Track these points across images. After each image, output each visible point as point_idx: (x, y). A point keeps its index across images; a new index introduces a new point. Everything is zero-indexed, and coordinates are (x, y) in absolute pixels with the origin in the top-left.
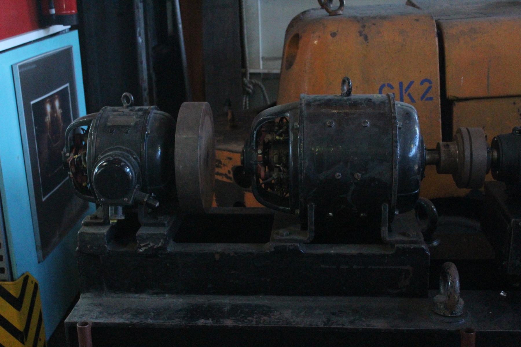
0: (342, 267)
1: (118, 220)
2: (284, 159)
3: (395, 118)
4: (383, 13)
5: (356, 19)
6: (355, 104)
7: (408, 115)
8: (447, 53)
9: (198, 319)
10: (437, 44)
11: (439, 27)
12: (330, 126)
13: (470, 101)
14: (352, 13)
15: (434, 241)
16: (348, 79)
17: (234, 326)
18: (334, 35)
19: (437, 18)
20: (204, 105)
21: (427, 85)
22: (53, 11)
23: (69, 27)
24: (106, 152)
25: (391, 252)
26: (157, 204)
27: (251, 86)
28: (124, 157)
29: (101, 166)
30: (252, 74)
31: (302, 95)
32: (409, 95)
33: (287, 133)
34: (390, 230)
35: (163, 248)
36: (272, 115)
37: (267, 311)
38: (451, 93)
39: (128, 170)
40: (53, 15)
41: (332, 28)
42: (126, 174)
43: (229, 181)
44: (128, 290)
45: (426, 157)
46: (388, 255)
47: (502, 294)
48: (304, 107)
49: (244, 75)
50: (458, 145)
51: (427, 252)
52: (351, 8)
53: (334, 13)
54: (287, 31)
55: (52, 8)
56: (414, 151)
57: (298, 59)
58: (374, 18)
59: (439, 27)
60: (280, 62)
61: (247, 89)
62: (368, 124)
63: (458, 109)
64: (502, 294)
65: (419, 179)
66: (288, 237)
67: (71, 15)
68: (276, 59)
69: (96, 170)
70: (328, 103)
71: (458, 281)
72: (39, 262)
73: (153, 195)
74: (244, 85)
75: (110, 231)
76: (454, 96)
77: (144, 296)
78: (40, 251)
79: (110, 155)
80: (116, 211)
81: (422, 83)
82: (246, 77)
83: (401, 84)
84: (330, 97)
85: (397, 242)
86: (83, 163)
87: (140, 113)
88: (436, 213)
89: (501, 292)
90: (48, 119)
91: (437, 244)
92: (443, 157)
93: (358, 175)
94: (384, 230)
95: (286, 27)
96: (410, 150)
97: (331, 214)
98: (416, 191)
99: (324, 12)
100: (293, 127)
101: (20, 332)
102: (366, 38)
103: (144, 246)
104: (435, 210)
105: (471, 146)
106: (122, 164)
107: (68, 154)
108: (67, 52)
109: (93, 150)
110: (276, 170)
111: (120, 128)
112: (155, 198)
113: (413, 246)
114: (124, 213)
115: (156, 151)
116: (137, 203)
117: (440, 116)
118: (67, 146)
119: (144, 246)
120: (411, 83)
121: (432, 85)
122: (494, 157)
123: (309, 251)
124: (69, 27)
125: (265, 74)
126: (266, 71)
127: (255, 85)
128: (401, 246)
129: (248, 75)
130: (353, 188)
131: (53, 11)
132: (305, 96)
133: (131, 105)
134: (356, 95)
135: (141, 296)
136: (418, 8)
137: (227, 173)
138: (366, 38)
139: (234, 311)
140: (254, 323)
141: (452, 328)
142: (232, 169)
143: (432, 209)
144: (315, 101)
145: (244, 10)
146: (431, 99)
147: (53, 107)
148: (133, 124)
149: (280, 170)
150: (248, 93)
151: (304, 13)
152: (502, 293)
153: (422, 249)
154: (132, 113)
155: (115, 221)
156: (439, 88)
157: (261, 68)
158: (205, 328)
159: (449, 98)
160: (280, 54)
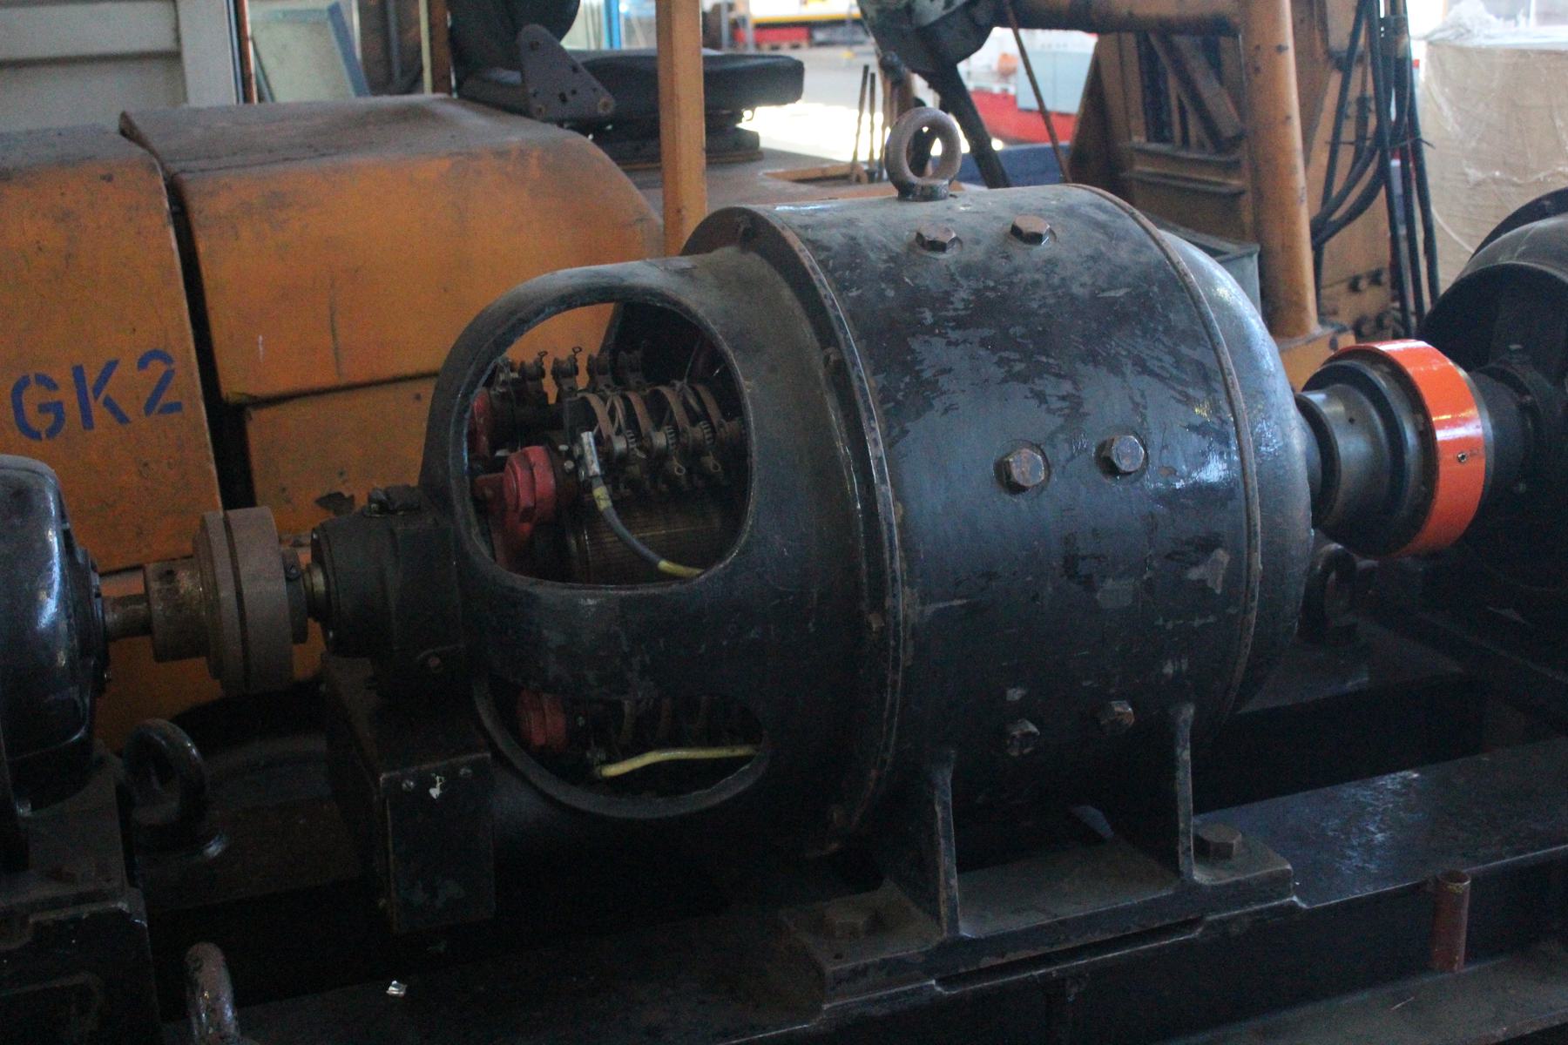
10: (174, 245)
13: (291, 403)
15: (208, 845)
21: (157, 368)
32: (108, 403)
45: (103, 618)
47: (393, 990)
50: (201, 570)
51: (137, 921)
63: (259, 428)
64: (393, 990)
65: (76, 697)
71: (227, 1006)
76: (244, 394)
81: (143, 363)
83: (78, 372)
88: (200, 760)
89: (390, 984)
91: (220, 850)
92: (158, 607)
96: (34, 606)
98: (76, 737)
104: (194, 751)
113: (85, 911)
117: (211, 454)
120: (111, 366)
121: (173, 366)
122: (315, 589)
143: (188, 750)
146: (175, 407)
152: (395, 986)
156: (197, 375)
159: (227, 398)
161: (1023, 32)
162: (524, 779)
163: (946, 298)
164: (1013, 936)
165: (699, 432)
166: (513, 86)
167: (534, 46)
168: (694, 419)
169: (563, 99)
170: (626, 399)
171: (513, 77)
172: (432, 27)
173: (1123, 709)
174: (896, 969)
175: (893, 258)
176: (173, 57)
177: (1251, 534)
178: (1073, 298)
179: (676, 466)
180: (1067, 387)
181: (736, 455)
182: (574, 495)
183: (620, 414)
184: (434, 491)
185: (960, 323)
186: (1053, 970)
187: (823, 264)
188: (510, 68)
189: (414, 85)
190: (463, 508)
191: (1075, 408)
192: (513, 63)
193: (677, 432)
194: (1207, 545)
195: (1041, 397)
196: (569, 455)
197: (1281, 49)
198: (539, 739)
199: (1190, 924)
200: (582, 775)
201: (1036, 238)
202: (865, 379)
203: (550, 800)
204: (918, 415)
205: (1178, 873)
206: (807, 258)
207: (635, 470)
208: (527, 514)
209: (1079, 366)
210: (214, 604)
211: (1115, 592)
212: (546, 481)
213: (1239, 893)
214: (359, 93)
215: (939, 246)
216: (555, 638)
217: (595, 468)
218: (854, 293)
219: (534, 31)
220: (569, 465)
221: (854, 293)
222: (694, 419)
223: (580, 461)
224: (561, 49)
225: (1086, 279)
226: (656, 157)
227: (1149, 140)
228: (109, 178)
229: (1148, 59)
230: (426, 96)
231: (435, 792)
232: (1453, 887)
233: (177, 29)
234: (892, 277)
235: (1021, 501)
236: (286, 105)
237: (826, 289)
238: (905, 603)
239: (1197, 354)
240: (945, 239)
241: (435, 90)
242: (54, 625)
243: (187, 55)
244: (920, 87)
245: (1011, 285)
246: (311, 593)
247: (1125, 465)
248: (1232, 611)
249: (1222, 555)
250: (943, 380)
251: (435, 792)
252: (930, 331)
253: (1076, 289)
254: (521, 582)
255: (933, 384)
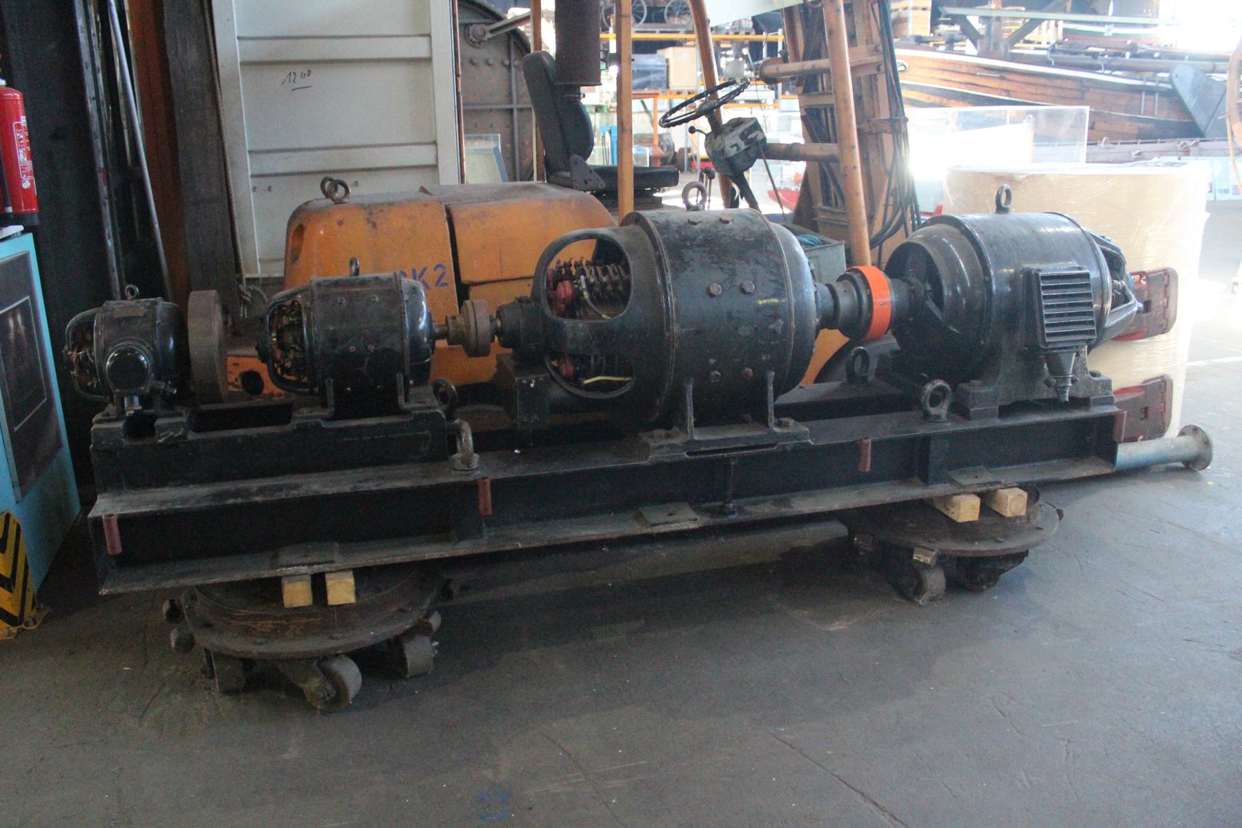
0: (364, 438)
1: (135, 411)
2: (298, 339)
3: (402, 292)
4: (391, 200)
5: (362, 207)
6: (363, 283)
7: (414, 290)
8: (458, 238)
9: (228, 499)
11: (448, 211)
12: (341, 303)
14: (359, 200)
16: (355, 260)
17: (264, 501)
18: (340, 223)
19: (447, 203)
20: (213, 293)
21: (440, 271)
22: (10, 210)
23: (21, 228)
24: (116, 343)
25: (407, 419)
26: (175, 392)
27: (249, 294)
28: (137, 347)
29: (113, 358)
30: (247, 279)
31: (312, 278)
33: (299, 314)
34: (406, 400)
35: (184, 436)
36: (283, 298)
37: (297, 487)
38: (466, 277)
39: (143, 359)
40: (10, 214)
41: (338, 217)
42: (141, 363)
43: (237, 390)
44: (150, 486)
46: (406, 423)
47: (516, 451)
48: (315, 289)
49: (240, 280)
52: (358, 196)
53: (338, 202)
54: (290, 224)
55: (8, 206)
56: (423, 324)
57: (304, 249)
58: (382, 204)
59: (448, 211)
60: (283, 263)
61: (244, 297)
62: (377, 299)
64: (516, 451)
66: (309, 415)
67: (32, 213)
68: (279, 260)
69: (108, 363)
70: (336, 284)
72: (17, 502)
73: (169, 382)
74: (240, 292)
75: (125, 425)
77: (167, 489)
78: (18, 490)
79: (123, 345)
80: (131, 402)
82: (241, 283)
83: (414, 271)
84: (339, 277)
85: (415, 409)
86: (90, 359)
87: (148, 304)
90: (12, 336)
93: (371, 348)
94: (401, 399)
95: (287, 218)
96: (419, 323)
97: (349, 389)
99: (329, 201)
100: (305, 307)
101: (7, 579)
102: (374, 225)
103: (163, 436)
105: (475, 316)
106: (137, 352)
107: (70, 353)
108: (23, 260)
109: (102, 343)
110: (292, 351)
111: (128, 319)
112: (172, 386)
113: (428, 412)
114: (141, 403)
115: (168, 342)
116: (154, 391)
118: (68, 343)
119: (163, 436)
120: (425, 269)
123: (330, 427)
124: (21, 228)
125: (264, 279)
126: (265, 275)
127: (254, 292)
128: (418, 412)
129: (245, 281)
130: (367, 359)
131: (10, 210)
132: (315, 278)
133: (137, 298)
134: (364, 275)
135: (164, 489)
136: (430, 194)
137: (234, 381)
138: (374, 225)
139: (261, 491)
140: (283, 496)
141: (471, 479)
142: (240, 375)
144: (325, 281)
145: (234, 204)
146: (446, 284)
147: (16, 323)
148: (142, 315)
149: (296, 351)
150: (245, 303)
151: (307, 203)
153: (437, 413)
154: (139, 305)
155: (132, 412)
157: (259, 272)
158: (235, 505)
160: (283, 254)
161: (767, 161)
162: (561, 386)
163: (694, 239)
164: (711, 441)
165: (616, 278)
166: (567, 178)
167: (576, 163)
168: (616, 274)
169: (586, 182)
170: (595, 268)
171: (567, 174)
172: (537, 156)
173: (749, 370)
174: (672, 446)
175: (679, 227)
176: (435, 167)
177: (791, 316)
178: (736, 240)
179: (609, 288)
180: (731, 266)
181: (627, 284)
182: (578, 294)
183: (593, 273)
184: (535, 297)
185: (698, 246)
186: (726, 455)
187: (657, 227)
188: (567, 171)
189: (531, 178)
190: (544, 301)
191: (733, 274)
192: (568, 169)
193: (610, 277)
194: (775, 317)
195: (722, 269)
196: (577, 283)
197: (855, 168)
198: (564, 373)
199: (773, 445)
200: (579, 386)
201: (727, 222)
202: (667, 262)
203: (569, 392)
204: (683, 272)
205: (768, 426)
206: (652, 225)
207: (597, 289)
208: (564, 301)
209: (736, 260)
210: (469, 327)
211: (745, 331)
212: (569, 291)
213: (788, 437)
214: (504, 181)
215: (695, 224)
216: (570, 335)
217: (584, 286)
218: (666, 236)
219: (575, 157)
220: (576, 286)
221: (666, 236)
222: (616, 274)
223: (580, 285)
224: (586, 165)
225: (742, 235)
226: (617, 206)
227: (824, 205)
228: (426, 205)
229: (822, 172)
230: (535, 181)
231: (532, 385)
232: (865, 441)
233: (437, 156)
234: (678, 232)
235: (714, 300)
236: (476, 187)
237: (657, 233)
238: (676, 328)
239: (776, 259)
240: (696, 221)
241: (538, 180)
242: (424, 327)
243: (440, 167)
244: (927, 218)
245: (716, 236)
246: (496, 327)
247: (748, 290)
248: (785, 340)
249: (781, 322)
250: (691, 263)
251: (532, 385)
252: (688, 248)
253: (737, 237)
254: (560, 319)
255: (688, 263)
